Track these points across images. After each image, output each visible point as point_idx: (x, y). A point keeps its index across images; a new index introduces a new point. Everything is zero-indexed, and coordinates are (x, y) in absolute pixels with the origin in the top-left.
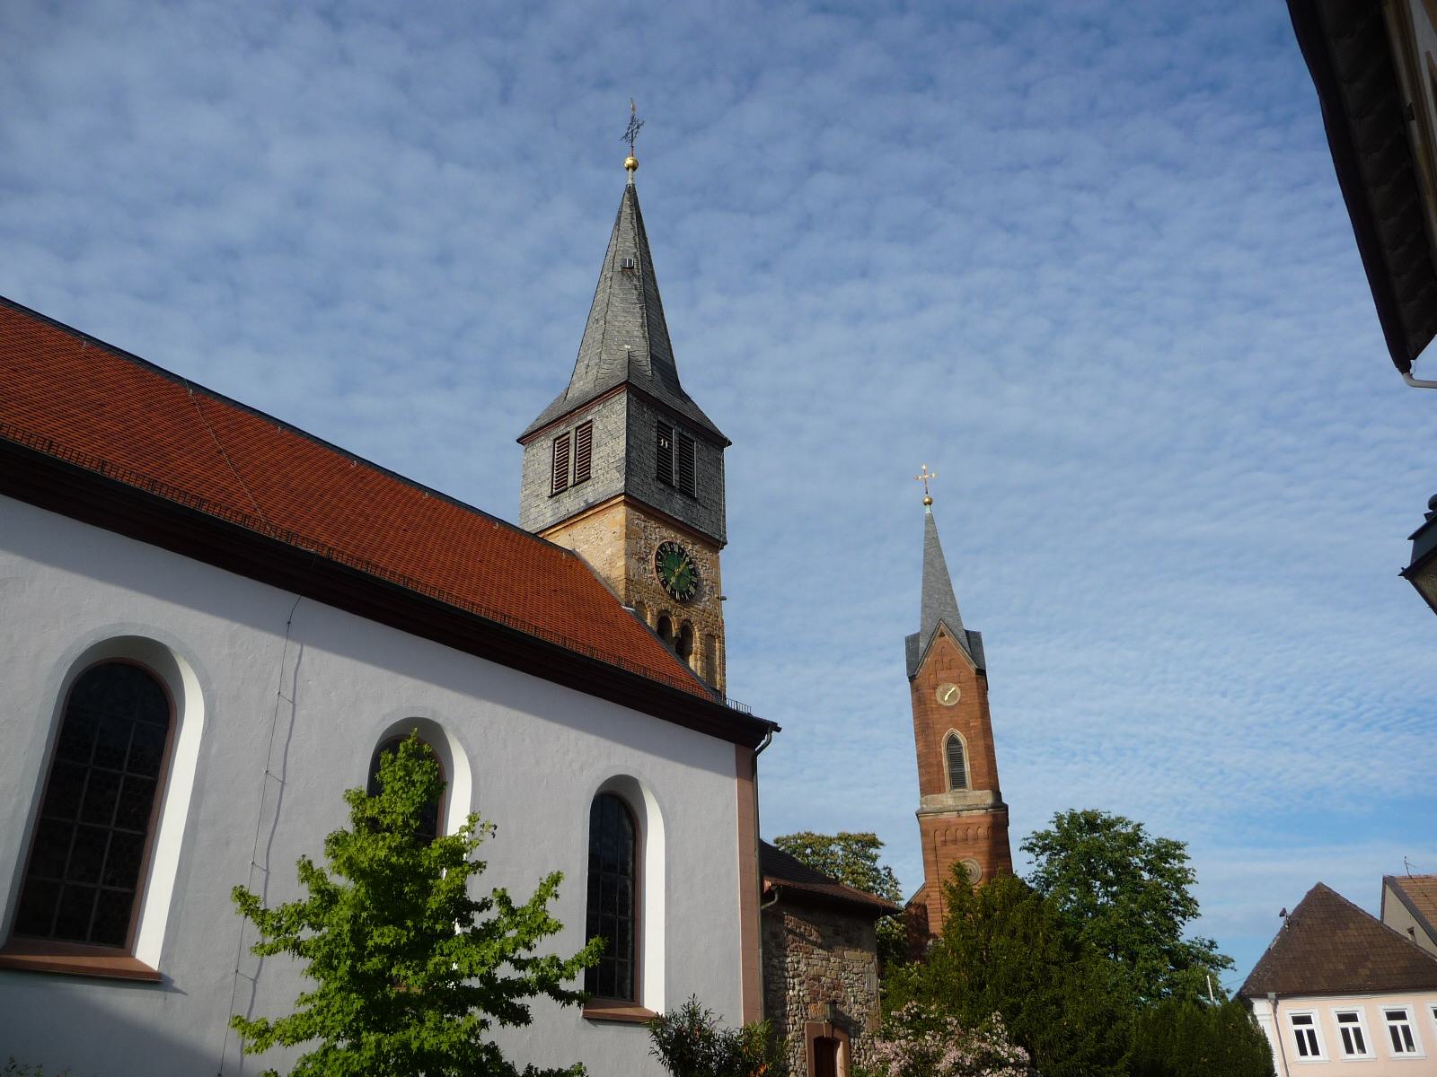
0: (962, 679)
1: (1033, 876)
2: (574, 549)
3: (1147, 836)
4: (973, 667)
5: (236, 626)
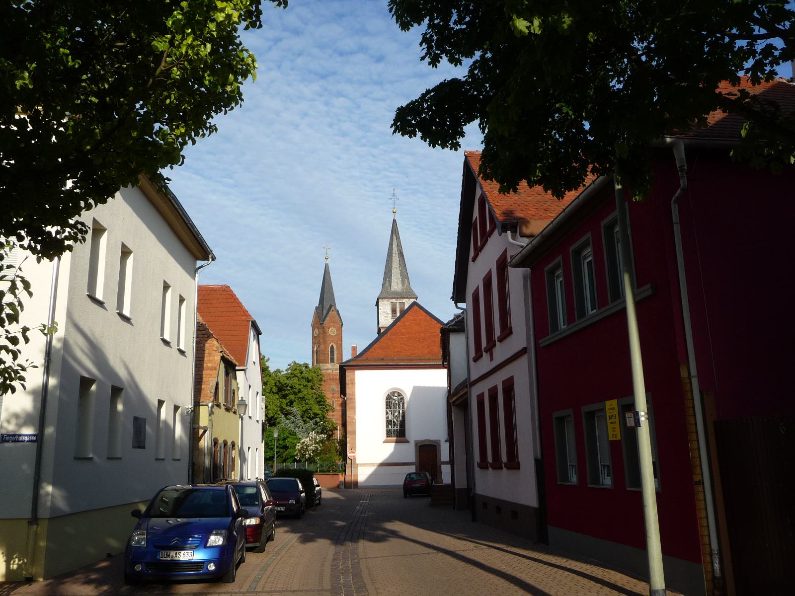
4: (341, 324)
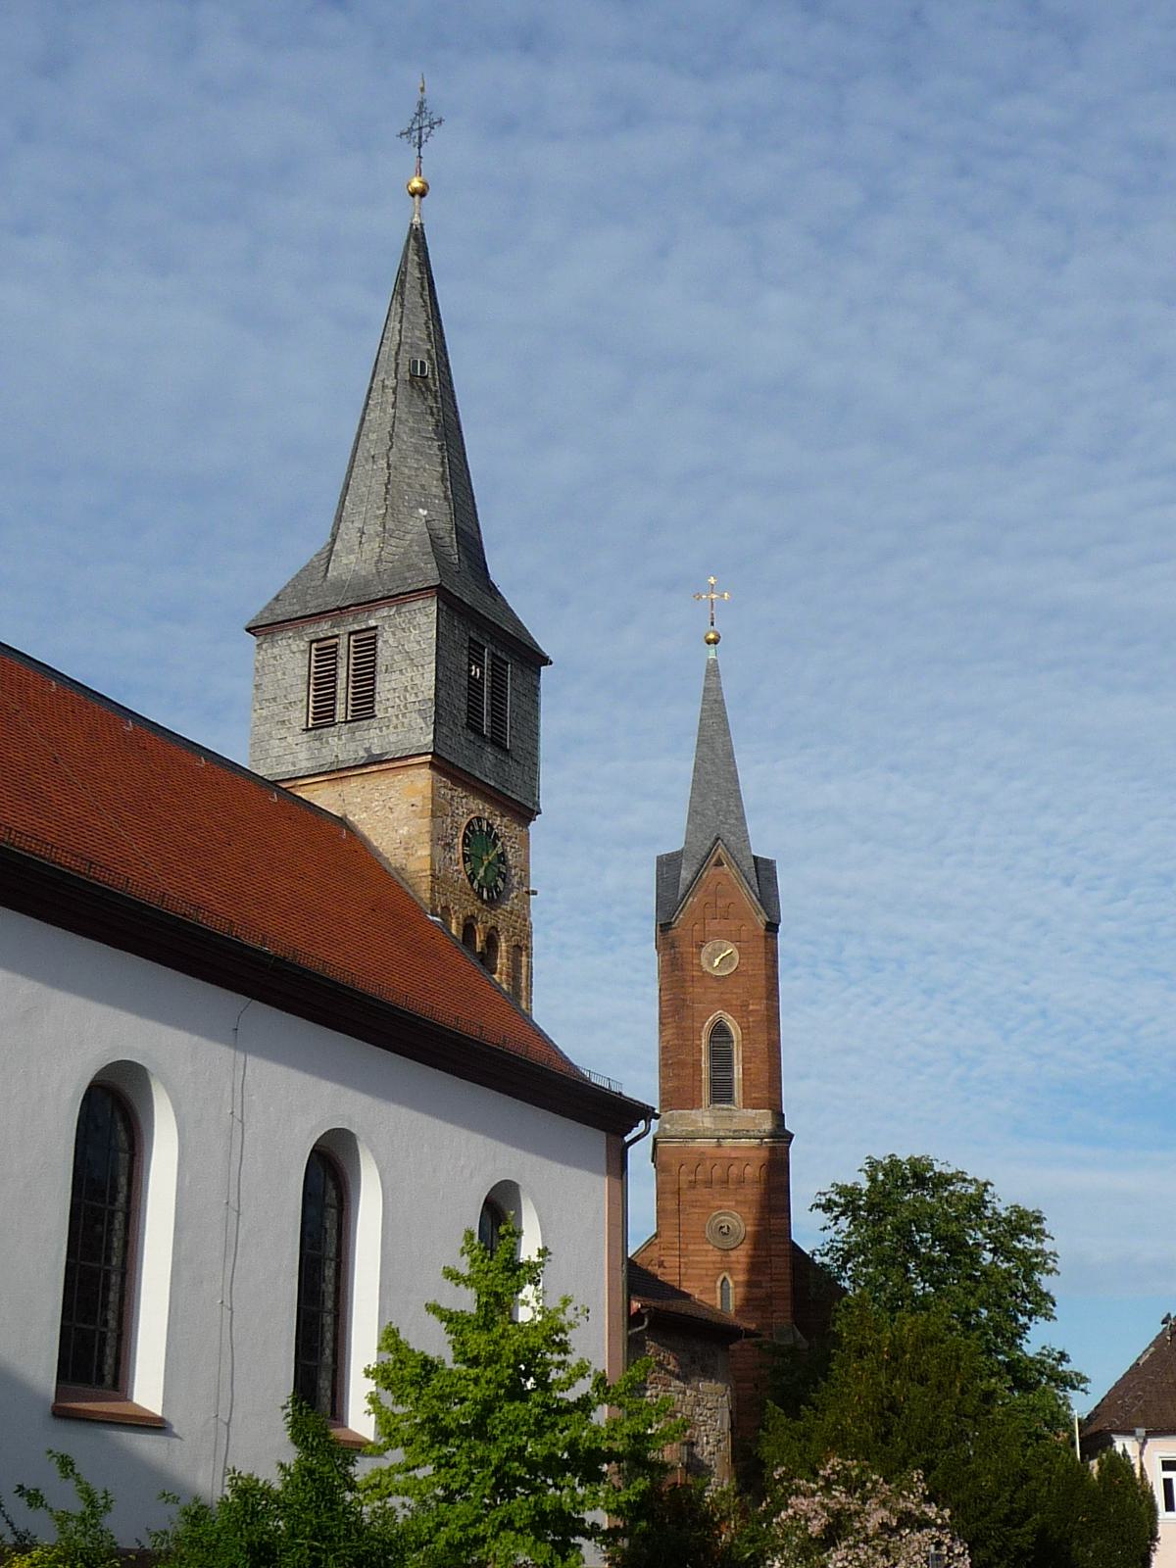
0: (744, 936)
1: (828, 1247)
2: (346, 816)
3: (996, 1200)
4: (761, 919)
5: (196, 1038)
